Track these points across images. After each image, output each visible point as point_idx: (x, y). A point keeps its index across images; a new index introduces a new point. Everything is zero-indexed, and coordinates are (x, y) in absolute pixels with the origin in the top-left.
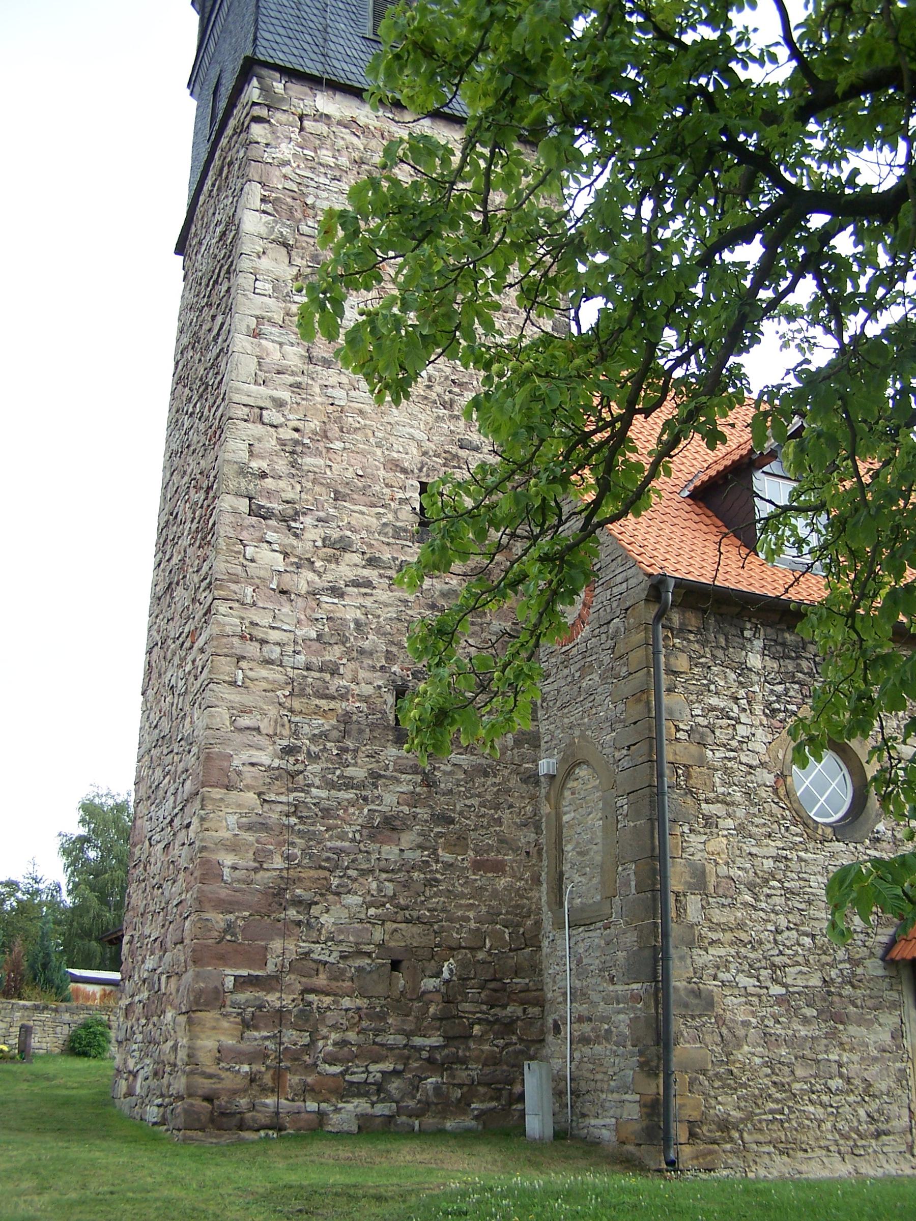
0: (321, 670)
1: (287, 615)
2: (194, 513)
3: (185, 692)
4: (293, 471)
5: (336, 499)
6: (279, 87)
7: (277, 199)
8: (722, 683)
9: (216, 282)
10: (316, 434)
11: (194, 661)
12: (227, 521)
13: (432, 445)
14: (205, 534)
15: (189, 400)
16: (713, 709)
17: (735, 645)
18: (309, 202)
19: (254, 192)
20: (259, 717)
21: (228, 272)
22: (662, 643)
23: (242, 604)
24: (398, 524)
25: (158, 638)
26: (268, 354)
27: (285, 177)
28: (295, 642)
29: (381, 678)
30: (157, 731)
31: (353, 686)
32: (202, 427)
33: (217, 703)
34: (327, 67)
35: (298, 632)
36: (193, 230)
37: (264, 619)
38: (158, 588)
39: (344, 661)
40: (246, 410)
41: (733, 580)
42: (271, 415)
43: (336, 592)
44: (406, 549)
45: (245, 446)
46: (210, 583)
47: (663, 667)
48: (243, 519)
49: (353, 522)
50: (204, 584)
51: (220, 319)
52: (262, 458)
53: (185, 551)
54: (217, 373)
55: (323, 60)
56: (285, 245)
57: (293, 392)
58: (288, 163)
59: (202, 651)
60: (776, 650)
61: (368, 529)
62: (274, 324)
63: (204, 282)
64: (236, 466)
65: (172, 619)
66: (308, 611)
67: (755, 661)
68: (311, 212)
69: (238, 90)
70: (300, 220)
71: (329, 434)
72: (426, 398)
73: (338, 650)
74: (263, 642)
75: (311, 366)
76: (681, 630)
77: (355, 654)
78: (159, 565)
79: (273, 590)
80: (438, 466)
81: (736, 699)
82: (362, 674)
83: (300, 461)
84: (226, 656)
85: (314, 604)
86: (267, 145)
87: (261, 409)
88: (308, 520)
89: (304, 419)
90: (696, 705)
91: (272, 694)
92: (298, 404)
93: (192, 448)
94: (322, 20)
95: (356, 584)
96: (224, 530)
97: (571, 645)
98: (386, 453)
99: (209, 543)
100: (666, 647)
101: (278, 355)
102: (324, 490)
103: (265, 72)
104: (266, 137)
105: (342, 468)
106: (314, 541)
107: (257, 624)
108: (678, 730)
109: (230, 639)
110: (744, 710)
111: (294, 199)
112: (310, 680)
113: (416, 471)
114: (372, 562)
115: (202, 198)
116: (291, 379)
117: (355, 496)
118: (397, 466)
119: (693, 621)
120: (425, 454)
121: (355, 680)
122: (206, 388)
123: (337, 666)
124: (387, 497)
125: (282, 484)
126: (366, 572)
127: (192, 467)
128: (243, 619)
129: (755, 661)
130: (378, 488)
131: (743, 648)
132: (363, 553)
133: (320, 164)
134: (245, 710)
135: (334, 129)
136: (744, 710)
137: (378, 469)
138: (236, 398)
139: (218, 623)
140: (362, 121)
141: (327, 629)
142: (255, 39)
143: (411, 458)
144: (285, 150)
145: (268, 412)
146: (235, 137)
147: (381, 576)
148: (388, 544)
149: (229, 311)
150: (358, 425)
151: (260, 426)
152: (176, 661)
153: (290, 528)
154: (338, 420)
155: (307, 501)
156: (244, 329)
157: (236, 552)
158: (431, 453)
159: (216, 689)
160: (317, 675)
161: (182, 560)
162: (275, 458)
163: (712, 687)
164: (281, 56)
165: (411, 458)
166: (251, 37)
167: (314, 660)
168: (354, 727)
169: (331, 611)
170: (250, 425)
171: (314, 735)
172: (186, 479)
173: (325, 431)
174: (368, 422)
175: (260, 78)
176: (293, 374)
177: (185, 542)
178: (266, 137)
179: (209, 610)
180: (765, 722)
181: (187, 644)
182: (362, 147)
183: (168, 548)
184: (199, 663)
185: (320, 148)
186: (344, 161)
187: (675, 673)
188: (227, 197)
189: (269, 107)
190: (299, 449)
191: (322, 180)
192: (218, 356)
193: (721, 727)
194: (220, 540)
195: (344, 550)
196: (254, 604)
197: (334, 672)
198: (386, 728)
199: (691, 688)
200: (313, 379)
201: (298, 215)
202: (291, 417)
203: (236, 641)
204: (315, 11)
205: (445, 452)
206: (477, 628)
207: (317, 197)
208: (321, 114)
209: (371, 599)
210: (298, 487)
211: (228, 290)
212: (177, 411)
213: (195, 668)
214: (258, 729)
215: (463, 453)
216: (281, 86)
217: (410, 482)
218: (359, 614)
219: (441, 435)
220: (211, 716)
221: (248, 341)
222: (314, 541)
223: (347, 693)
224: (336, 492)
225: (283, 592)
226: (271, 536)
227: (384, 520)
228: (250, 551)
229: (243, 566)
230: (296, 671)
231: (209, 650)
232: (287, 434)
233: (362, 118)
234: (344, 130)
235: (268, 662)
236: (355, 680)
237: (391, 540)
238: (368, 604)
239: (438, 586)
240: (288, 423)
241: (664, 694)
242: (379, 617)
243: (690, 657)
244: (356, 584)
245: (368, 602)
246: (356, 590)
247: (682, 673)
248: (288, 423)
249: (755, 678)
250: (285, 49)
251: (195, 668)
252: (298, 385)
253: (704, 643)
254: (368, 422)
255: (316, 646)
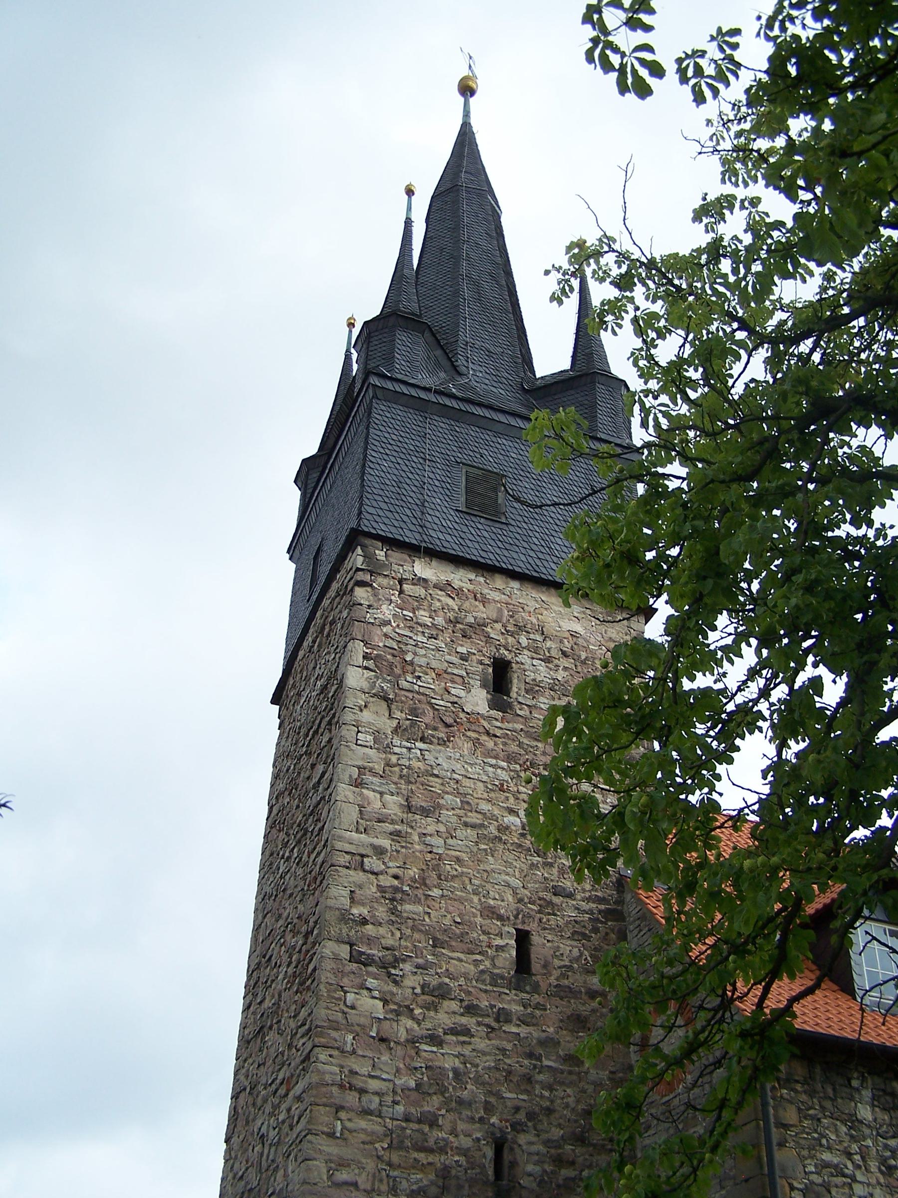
0: (419, 1121)
1: (386, 1064)
2: (290, 957)
3: (279, 1142)
4: (393, 918)
5: (434, 946)
6: (380, 554)
7: (378, 656)
8: (833, 1137)
9: (316, 732)
10: (415, 881)
11: (289, 1110)
12: (328, 968)
13: (527, 892)
14: (304, 979)
15: (285, 845)
16: (826, 1165)
17: (844, 1095)
18: (408, 659)
19: (358, 649)
20: (357, 1171)
21: (330, 723)
22: (770, 1094)
23: (343, 1052)
24: (496, 971)
25: (247, 1083)
26: (369, 804)
27: (386, 635)
28: (394, 1092)
29: (480, 1130)
30: (243, 1183)
31: (452, 1138)
32: (300, 872)
33: (315, 1156)
34: (424, 536)
35: (397, 1082)
36: (291, 681)
37: (364, 1069)
38: (246, 1032)
39: (443, 1112)
40: (348, 857)
41: (824, 1025)
42: (372, 863)
43: (435, 1040)
44: (503, 996)
45: (346, 893)
46: (310, 1030)
47: (772, 1120)
48: (344, 965)
49: (451, 969)
50: (302, 1031)
51: (320, 768)
52: (363, 905)
53: (280, 996)
54: (318, 820)
55: (421, 531)
56: (386, 699)
57: (393, 840)
58: (389, 623)
59: (299, 1099)
60: (885, 1100)
61: (465, 976)
62: (375, 774)
63: (303, 731)
64: (337, 912)
65: (264, 1064)
66: (407, 1059)
67: (865, 1112)
68: (409, 668)
69: (342, 557)
70: (400, 676)
71: (428, 882)
72: (520, 846)
73: (436, 1100)
74: (362, 1091)
75: (410, 815)
76: (788, 1080)
77: (454, 1104)
78: (249, 1007)
79: (373, 1037)
80: (533, 913)
81: (849, 1155)
82: (461, 1126)
83: (399, 908)
84: (325, 1105)
85: (413, 1053)
86: (369, 606)
87: (363, 856)
88: (407, 967)
89: (404, 867)
90: (808, 1161)
91: (371, 1147)
92: (398, 852)
93: (289, 892)
94: (420, 496)
95: (454, 1031)
96: (326, 976)
97: (671, 1096)
98: (483, 900)
99: (308, 988)
100: (774, 1098)
101: (378, 805)
102: (422, 937)
103: (368, 541)
104: (368, 599)
105: (440, 915)
106: (414, 988)
107: (356, 1073)
108: (792, 1188)
109: (329, 1088)
110: (859, 1167)
111: (394, 656)
112: (408, 1132)
113: (512, 918)
114: (471, 1010)
115: (301, 653)
116: (390, 828)
117: (453, 944)
118: (493, 913)
119: (800, 1070)
120: (520, 901)
121: (454, 1132)
122: (305, 834)
123: (436, 1117)
124: (484, 944)
125: (382, 931)
126: (464, 1020)
127: (288, 911)
128: (342, 1067)
129: (865, 1112)
130: (475, 935)
131: (852, 1099)
132: (461, 1001)
133: (417, 623)
134: (343, 1164)
135: (431, 592)
136: (859, 1167)
137: (475, 916)
138: (339, 845)
139: (318, 1071)
140: (457, 584)
141: (425, 1079)
142: (360, 513)
143: (507, 904)
144: (387, 611)
145: (370, 859)
146: (338, 599)
147: (479, 1024)
148: (486, 991)
149: (331, 760)
150: (455, 873)
151: (361, 874)
152: (268, 1108)
153: (389, 975)
154: (436, 868)
155: (406, 947)
156: (347, 780)
157: (337, 999)
158: (526, 900)
159: (314, 1141)
160: (415, 1126)
161: (277, 1004)
162: (375, 905)
163: (824, 1141)
164: (383, 527)
165: (507, 904)
166: (356, 512)
167: (413, 1110)
168: (453, 1182)
169: (431, 1060)
170: (351, 872)
171: (413, 1191)
172: (281, 922)
173: (424, 879)
174: (465, 870)
175: (364, 547)
176: (393, 822)
177: (280, 985)
178: (368, 599)
179: (308, 1057)
180: (882, 1181)
181: (282, 1091)
182: (456, 608)
183: (260, 990)
184: (295, 1112)
185: (418, 609)
186: (440, 620)
187: (786, 1127)
188: (329, 653)
189: (372, 573)
190: (399, 896)
191: (420, 638)
192: (319, 803)
193: (837, 1186)
194: (322, 987)
195: (443, 997)
196: (354, 1052)
197: (433, 1123)
198: (486, 1183)
199: (803, 1142)
200: (412, 827)
201: (398, 671)
202: (391, 864)
203: (335, 1090)
204: (414, 489)
205: (540, 899)
206: (574, 1077)
207: (415, 654)
208: (420, 578)
209: (470, 1048)
210: (398, 935)
211: (330, 741)
212: (272, 854)
213: (290, 1117)
214: (355, 1185)
215: (557, 900)
216: (383, 553)
217: (506, 929)
218: (457, 1063)
219: (535, 882)
220: (309, 1169)
221: (350, 790)
222: (414, 988)
223: (446, 1145)
224: (435, 939)
225: (382, 1040)
226: (371, 982)
227: (482, 967)
228: (350, 997)
229: (344, 1013)
230: (395, 1123)
231: (308, 1099)
232: (387, 881)
233: (456, 582)
234: (440, 592)
235: (366, 1112)
236: (454, 1132)
237: (489, 988)
238: (467, 1053)
239: (535, 1034)
240: (388, 870)
241: (775, 1148)
242: (477, 1066)
243: (799, 1109)
244: (454, 1031)
245: (467, 1051)
246: (454, 1038)
247: (792, 1126)
248: (388, 870)
249: (867, 1131)
250: (386, 521)
251: (290, 1117)
252: (398, 833)
253: (812, 1094)
254: (465, 870)
255: (414, 1095)
